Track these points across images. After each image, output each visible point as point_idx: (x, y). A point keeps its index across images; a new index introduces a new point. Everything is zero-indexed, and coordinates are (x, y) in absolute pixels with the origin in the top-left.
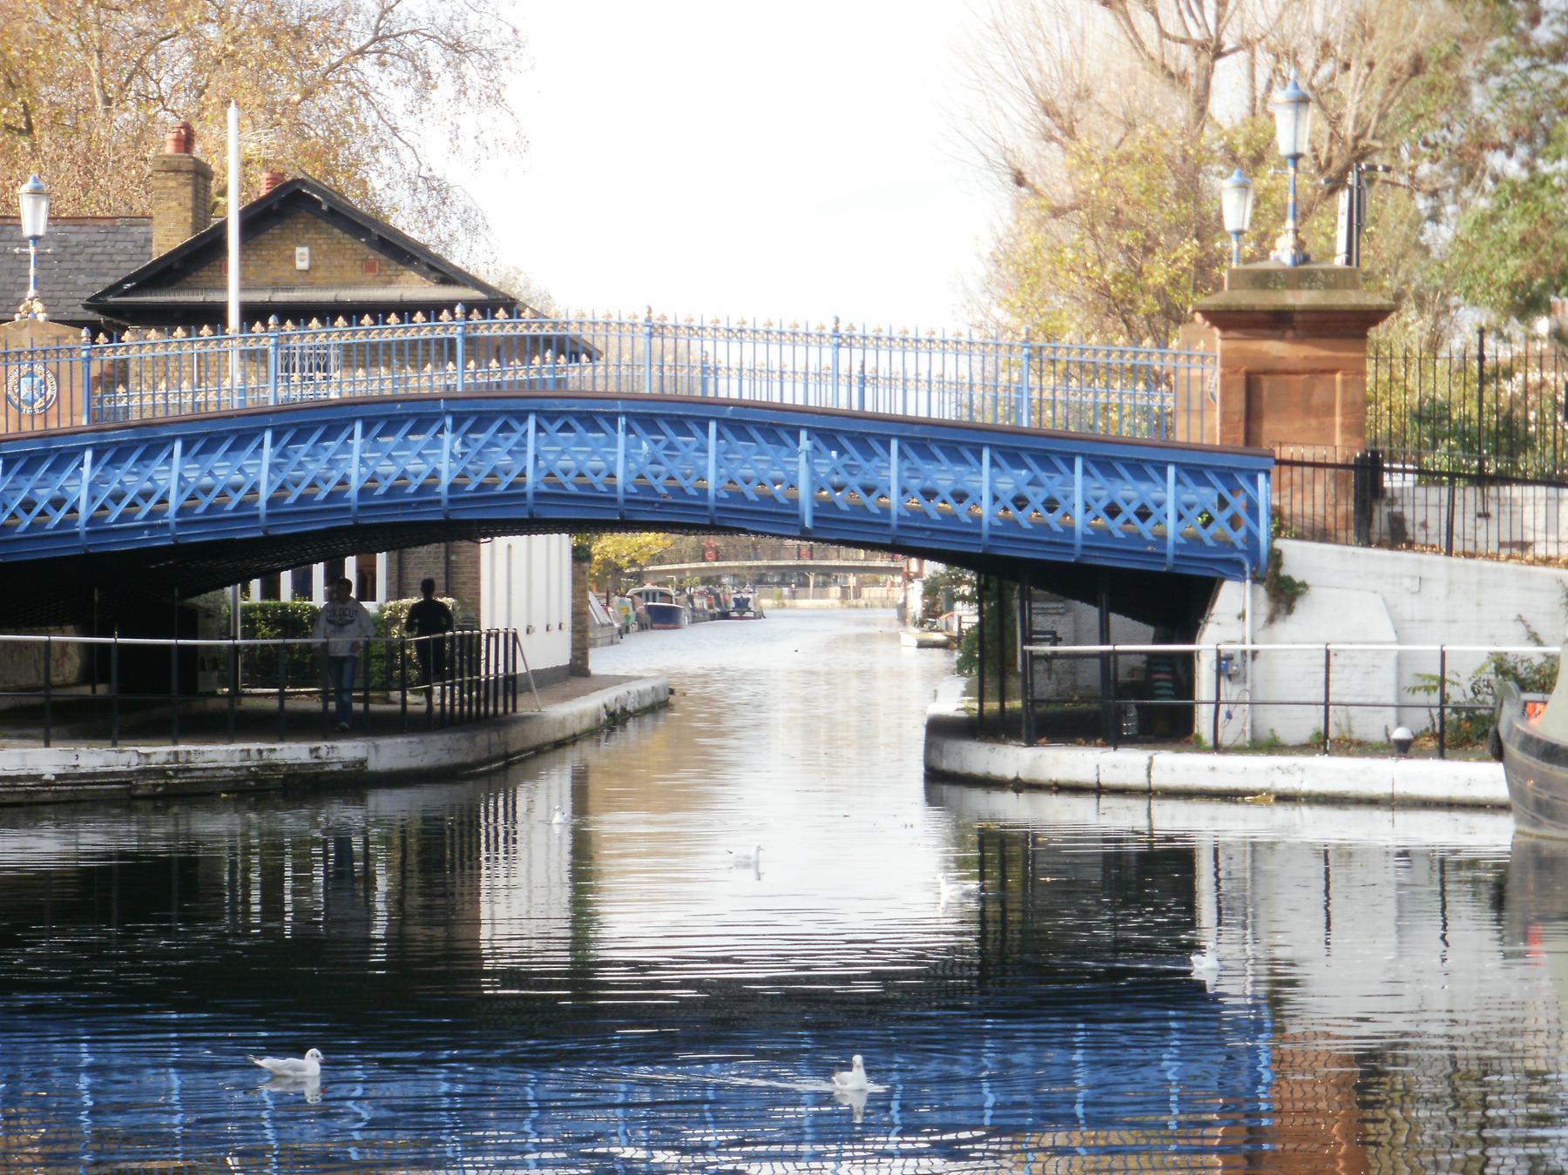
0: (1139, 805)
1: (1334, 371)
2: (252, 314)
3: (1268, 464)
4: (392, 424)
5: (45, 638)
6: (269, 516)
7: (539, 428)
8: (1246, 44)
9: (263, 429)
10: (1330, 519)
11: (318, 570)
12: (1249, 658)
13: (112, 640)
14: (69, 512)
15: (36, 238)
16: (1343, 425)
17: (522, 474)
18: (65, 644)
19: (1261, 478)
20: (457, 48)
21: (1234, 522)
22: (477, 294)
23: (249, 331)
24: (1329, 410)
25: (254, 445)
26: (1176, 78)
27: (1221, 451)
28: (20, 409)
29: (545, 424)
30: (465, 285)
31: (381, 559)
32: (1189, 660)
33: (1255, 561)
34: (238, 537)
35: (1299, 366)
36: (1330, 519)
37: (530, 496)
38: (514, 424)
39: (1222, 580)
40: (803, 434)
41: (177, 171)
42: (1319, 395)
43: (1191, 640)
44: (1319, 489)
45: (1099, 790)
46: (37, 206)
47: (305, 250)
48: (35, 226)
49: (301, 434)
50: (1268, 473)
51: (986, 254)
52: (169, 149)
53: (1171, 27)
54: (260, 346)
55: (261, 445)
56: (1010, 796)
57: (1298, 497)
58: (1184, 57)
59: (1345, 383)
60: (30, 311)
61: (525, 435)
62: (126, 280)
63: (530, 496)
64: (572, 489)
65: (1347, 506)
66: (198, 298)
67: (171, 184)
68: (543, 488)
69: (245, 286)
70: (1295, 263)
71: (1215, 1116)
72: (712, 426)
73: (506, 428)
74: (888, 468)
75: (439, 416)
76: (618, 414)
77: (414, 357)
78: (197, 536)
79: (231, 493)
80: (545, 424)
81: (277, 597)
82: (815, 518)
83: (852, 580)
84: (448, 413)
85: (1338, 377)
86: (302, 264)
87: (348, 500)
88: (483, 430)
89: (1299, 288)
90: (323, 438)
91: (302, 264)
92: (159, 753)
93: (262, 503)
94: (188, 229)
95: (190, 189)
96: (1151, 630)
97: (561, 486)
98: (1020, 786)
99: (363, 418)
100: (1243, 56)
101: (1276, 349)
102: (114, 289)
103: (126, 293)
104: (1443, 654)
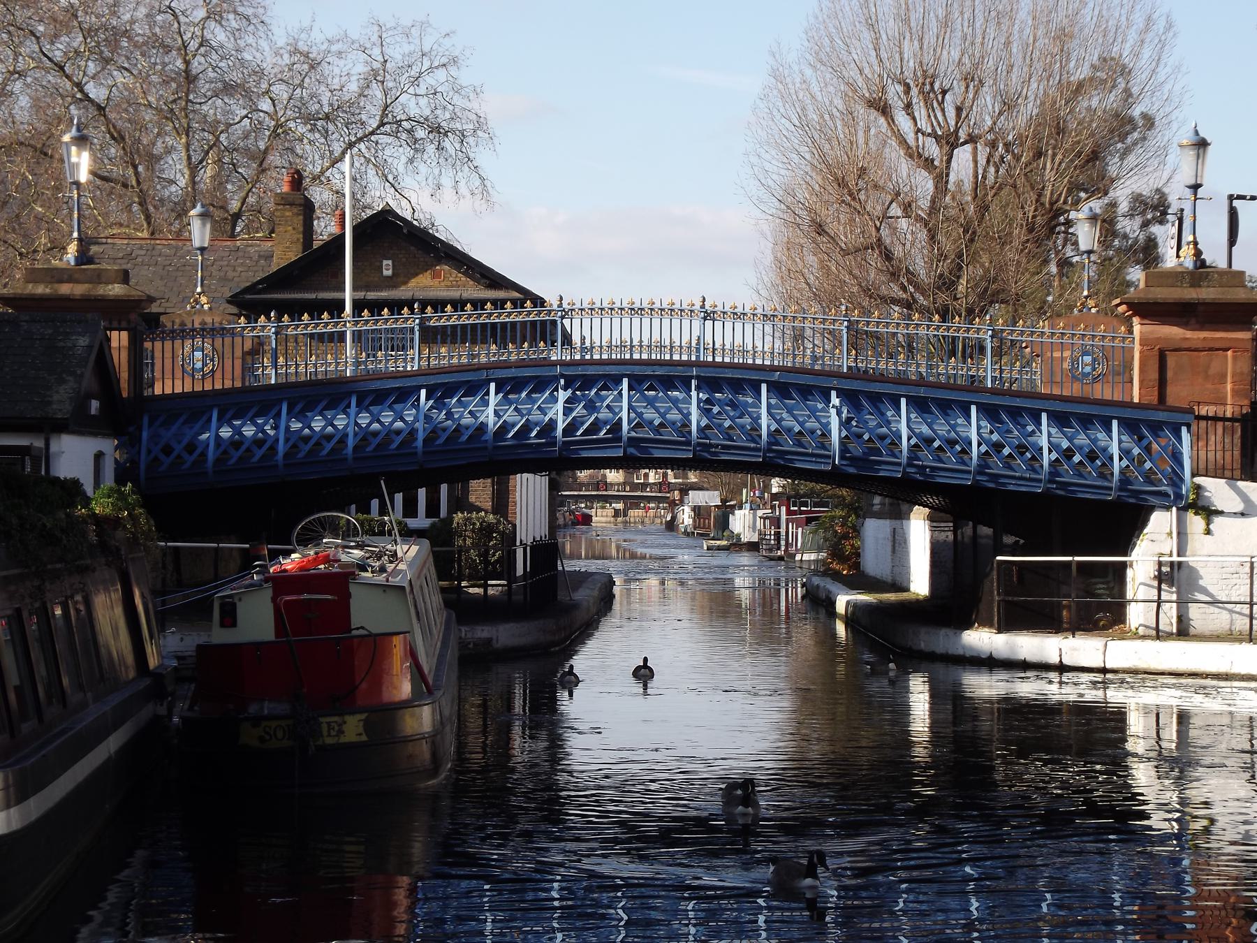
1: (1227, 350)
3: (1188, 418)
5: (1070, 558)
6: (424, 453)
8: (972, 139)
9: (280, 401)
11: (422, 493)
12: (1176, 567)
13: (1077, 558)
15: (202, 249)
16: (1233, 390)
18: (232, 549)
19: (1184, 429)
20: (436, 129)
22: (516, 295)
23: (360, 316)
24: (1222, 378)
25: (205, 418)
26: (928, 163)
27: (1139, 406)
28: (193, 376)
29: (636, 386)
30: (507, 288)
31: (444, 488)
32: (1120, 571)
34: (400, 469)
35: (1200, 346)
39: (1151, 509)
41: (291, 204)
42: (1215, 368)
43: (1125, 554)
46: (204, 225)
47: (390, 262)
48: (202, 240)
49: (449, 390)
50: (1189, 426)
52: (286, 188)
53: (923, 124)
54: (408, 324)
58: (933, 149)
59: (1235, 358)
60: (197, 302)
67: (287, 214)
69: (355, 288)
70: (1196, 267)
71: (1188, 926)
73: (605, 388)
74: (899, 422)
75: (556, 379)
76: (692, 377)
77: (494, 336)
79: (324, 443)
81: (369, 512)
83: (620, 506)
84: (562, 376)
85: (1229, 353)
86: (388, 272)
87: (416, 447)
89: (1200, 286)
91: (388, 272)
93: (419, 443)
94: (300, 247)
95: (301, 217)
98: (1042, 667)
100: (968, 147)
101: (1173, 332)
102: (251, 289)
103: (259, 292)
104: (1252, 563)
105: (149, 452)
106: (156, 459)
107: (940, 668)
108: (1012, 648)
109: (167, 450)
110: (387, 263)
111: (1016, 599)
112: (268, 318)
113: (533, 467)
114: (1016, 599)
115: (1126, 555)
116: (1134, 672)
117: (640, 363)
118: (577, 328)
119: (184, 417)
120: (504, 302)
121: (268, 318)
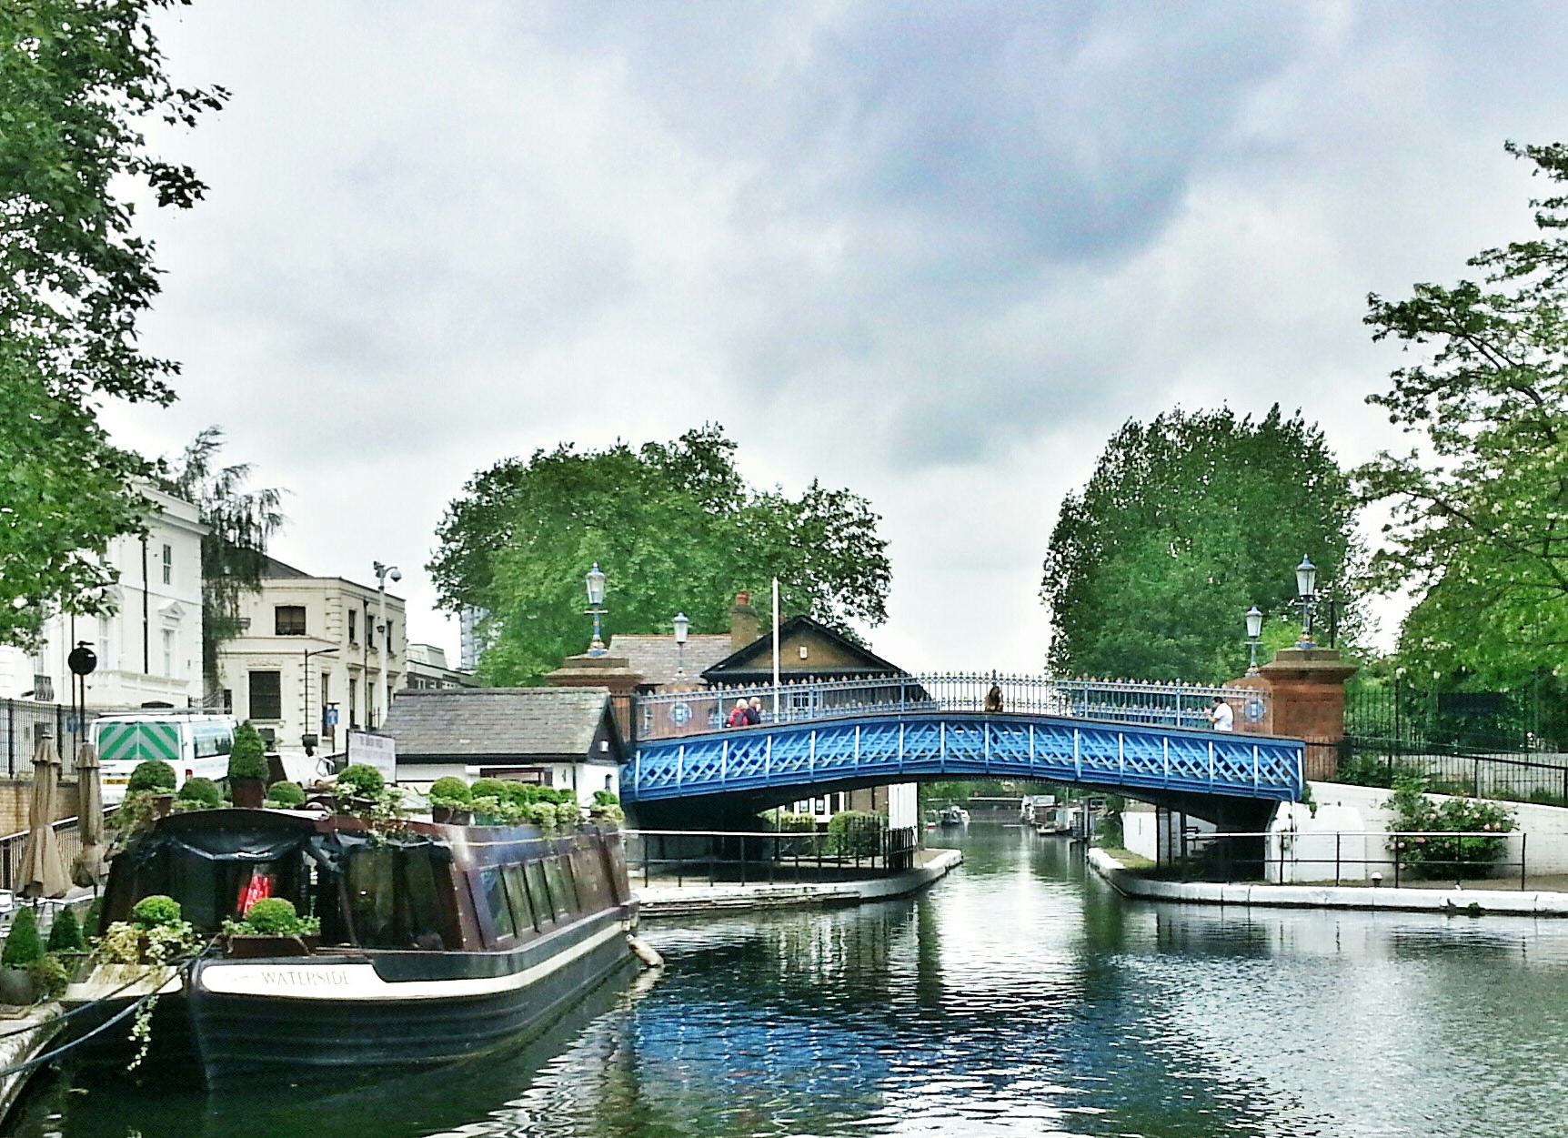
0: (1244, 910)
2: (784, 678)
4: (830, 732)
7: (946, 729)
10: (1327, 772)
14: (761, 766)
17: (939, 751)
21: (1286, 773)
25: (675, 753)
29: (949, 727)
31: (842, 795)
32: (1261, 843)
33: (1297, 791)
36: (1327, 772)
37: (943, 763)
38: (934, 727)
40: (1076, 731)
44: (1321, 757)
45: (1222, 903)
47: (805, 649)
51: (381, 772)
55: (678, 753)
56: (1197, 907)
57: (1311, 761)
61: (939, 732)
62: (720, 664)
63: (943, 763)
64: (962, 758)
65: (1334, 766)
66: (753, 672)
68: (949, 759)
72: (1031, 728)
73: (930, 729)
75: (898, 723)
78: (685, 793)
80: (949, 727)
82: (1082, 773)
88: (889, 732)
90: (707, 750)
92: (766, 888)
93: (856, 761)
96: (1215, 826)
97: (972, 757)
99: (859, 725)
103: (721, 669)
105: (641, 774)
106: (645, 779)
107: (1162, 907)
108: (1188, 891)
109: (652, 773)
110: (803, 649)
111: (193, 850)
112: (717, 687)
113: (902, 779)
114: (193, 850)
115: (1264, 832)
116: (1507, 915)
117: (955, 713)
118: (930, 688)
119: (706, 747)
120: (854, 674)
121: (717, 687)
